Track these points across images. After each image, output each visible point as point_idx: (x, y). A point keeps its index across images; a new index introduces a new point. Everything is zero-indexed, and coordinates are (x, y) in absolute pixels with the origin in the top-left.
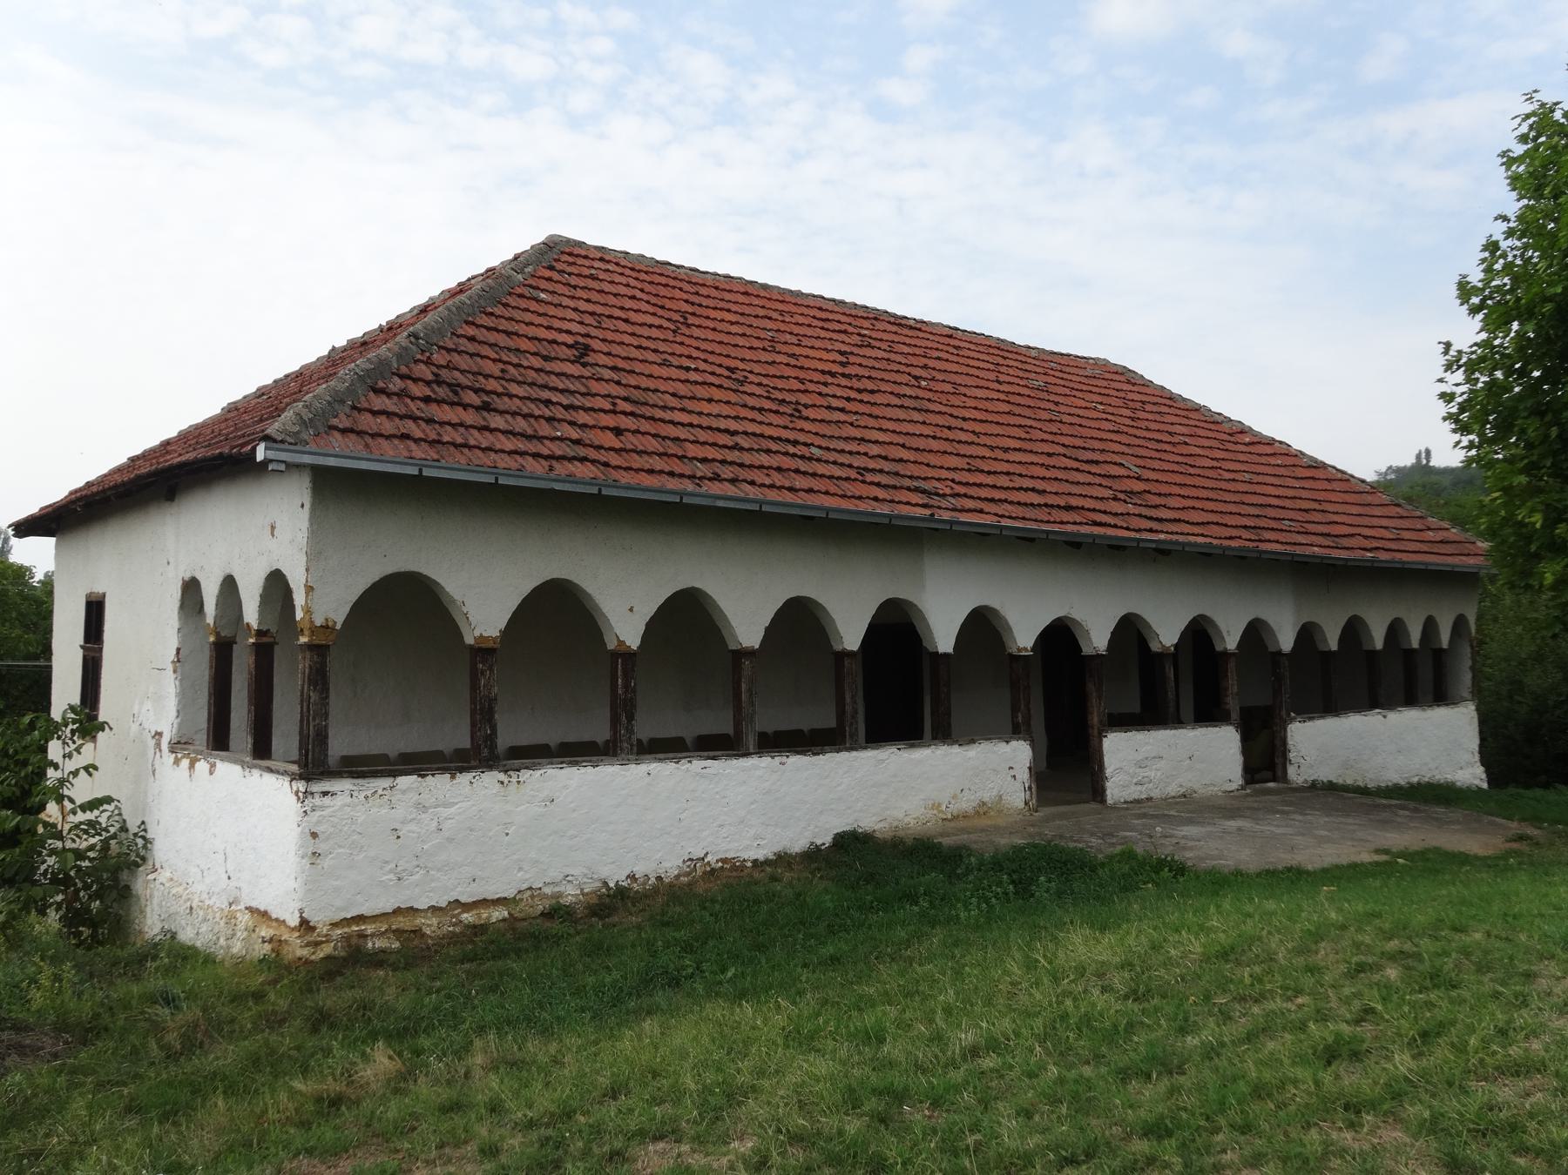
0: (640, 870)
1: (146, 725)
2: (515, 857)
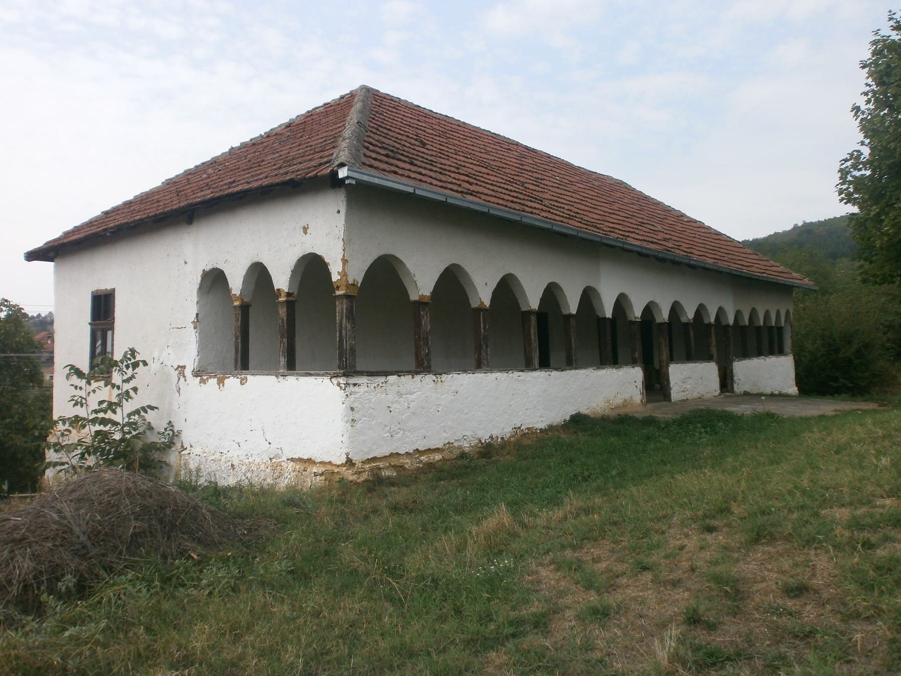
0: (495, 433)
1: (166, 362)
2: (442, 424)
